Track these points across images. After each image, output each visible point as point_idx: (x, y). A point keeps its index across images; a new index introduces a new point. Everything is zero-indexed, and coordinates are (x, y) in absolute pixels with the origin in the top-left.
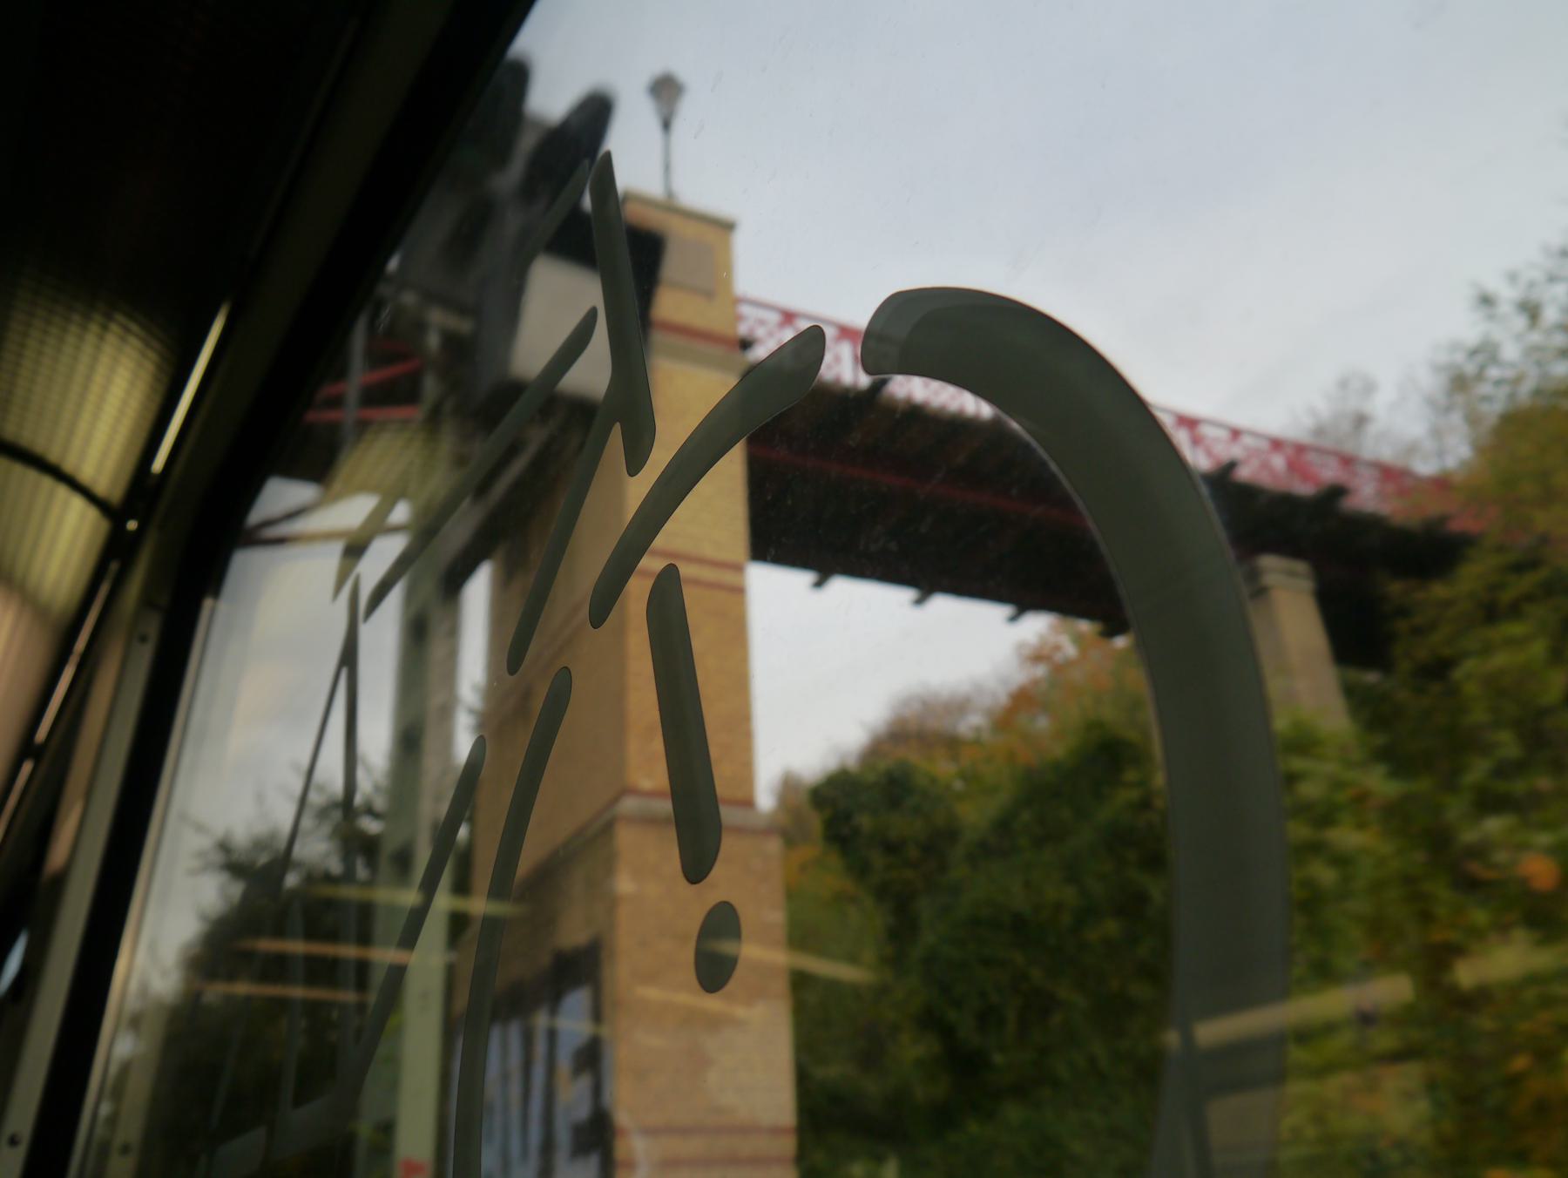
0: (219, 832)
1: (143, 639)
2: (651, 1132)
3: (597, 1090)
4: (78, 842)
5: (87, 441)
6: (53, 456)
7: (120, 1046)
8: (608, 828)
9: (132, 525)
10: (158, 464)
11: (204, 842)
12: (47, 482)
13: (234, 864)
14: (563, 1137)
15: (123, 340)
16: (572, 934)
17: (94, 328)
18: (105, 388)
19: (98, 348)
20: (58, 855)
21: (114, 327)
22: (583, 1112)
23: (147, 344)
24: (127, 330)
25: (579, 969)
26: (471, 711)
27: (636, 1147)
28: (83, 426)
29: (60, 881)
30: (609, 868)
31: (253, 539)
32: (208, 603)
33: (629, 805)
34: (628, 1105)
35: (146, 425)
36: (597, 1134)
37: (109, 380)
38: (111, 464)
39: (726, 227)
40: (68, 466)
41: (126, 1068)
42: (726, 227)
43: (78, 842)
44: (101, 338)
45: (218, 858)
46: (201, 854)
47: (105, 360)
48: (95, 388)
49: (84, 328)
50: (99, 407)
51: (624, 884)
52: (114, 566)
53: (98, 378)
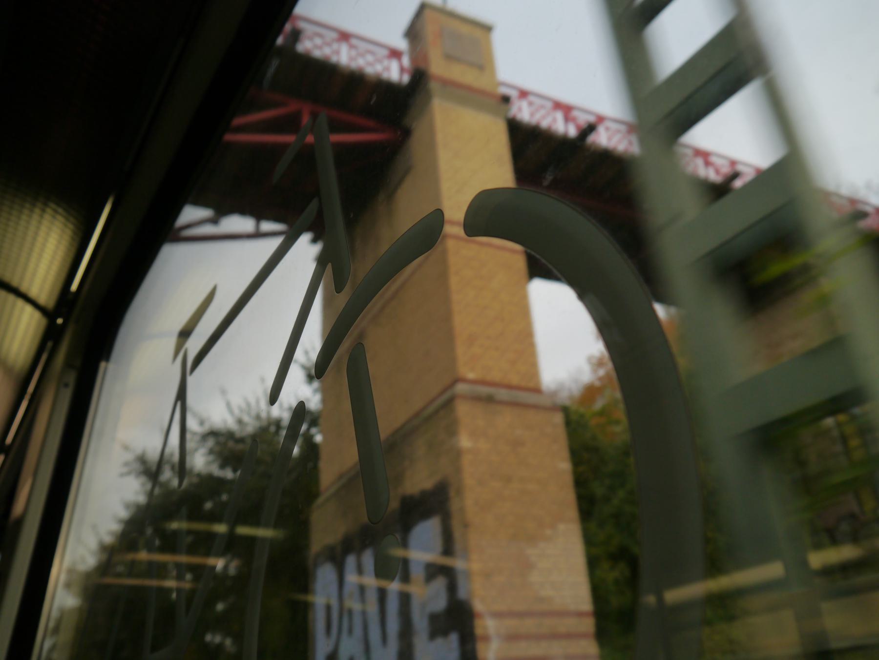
0: (139, 451)
1: (66, 385)
2: (498, 615)
3: (452, 588)
4: (30, 500)
5: (34, 275)
6: (15, 283)
7: (62, 598)
8: (449, 404)
9: (60, 321)
10: (74, 287)
11: (129, 457)
12: (11, 297)
13: (151, 471)
14: (420, 623)
15: (54, 217)
16: (418, 480)
17: (37, 211)
18: (44, 245)
19: (40, 222)
20: (18, 508)
21: (49, 211)
22: (440, 604)
23: (67, 219)
24: (56, 211)
25: (434, 503)
26: (304, 367)
27: (488, 625)
28: (31, 266)
29: (20, 522)
30: (452, 430)
31: (177, 237)
32: (103, 365)
33: (461, 388)
34: (482, 598)
35: (65, 270)
36: (457, 619)
37: (46, 240)
38: (47, 287)
39: (488, 29)
40: (24, 288)
41: (63, 613)
42: (488, 29)
43: (30, 500)
44: (42, 216)
45: (137, 466)
46: (126, 464)
47: (43, 229)
48: (38, 244)
49: (32, 211)
50: (40, 256)
51: (465, 442)
52: (50, 344)
53: (40, 239)
